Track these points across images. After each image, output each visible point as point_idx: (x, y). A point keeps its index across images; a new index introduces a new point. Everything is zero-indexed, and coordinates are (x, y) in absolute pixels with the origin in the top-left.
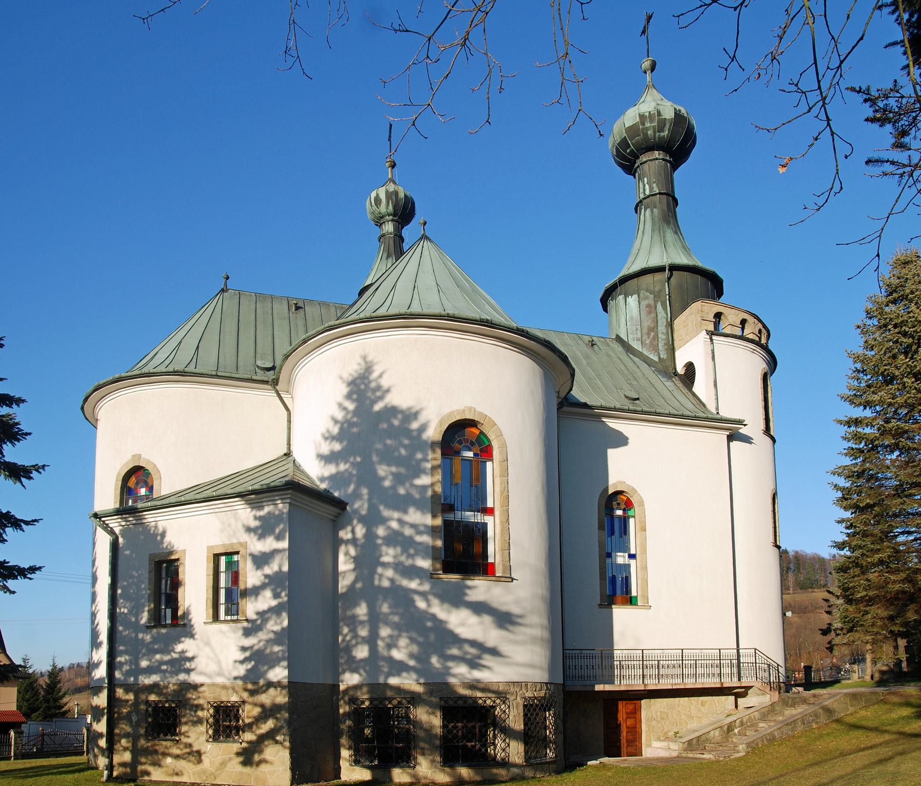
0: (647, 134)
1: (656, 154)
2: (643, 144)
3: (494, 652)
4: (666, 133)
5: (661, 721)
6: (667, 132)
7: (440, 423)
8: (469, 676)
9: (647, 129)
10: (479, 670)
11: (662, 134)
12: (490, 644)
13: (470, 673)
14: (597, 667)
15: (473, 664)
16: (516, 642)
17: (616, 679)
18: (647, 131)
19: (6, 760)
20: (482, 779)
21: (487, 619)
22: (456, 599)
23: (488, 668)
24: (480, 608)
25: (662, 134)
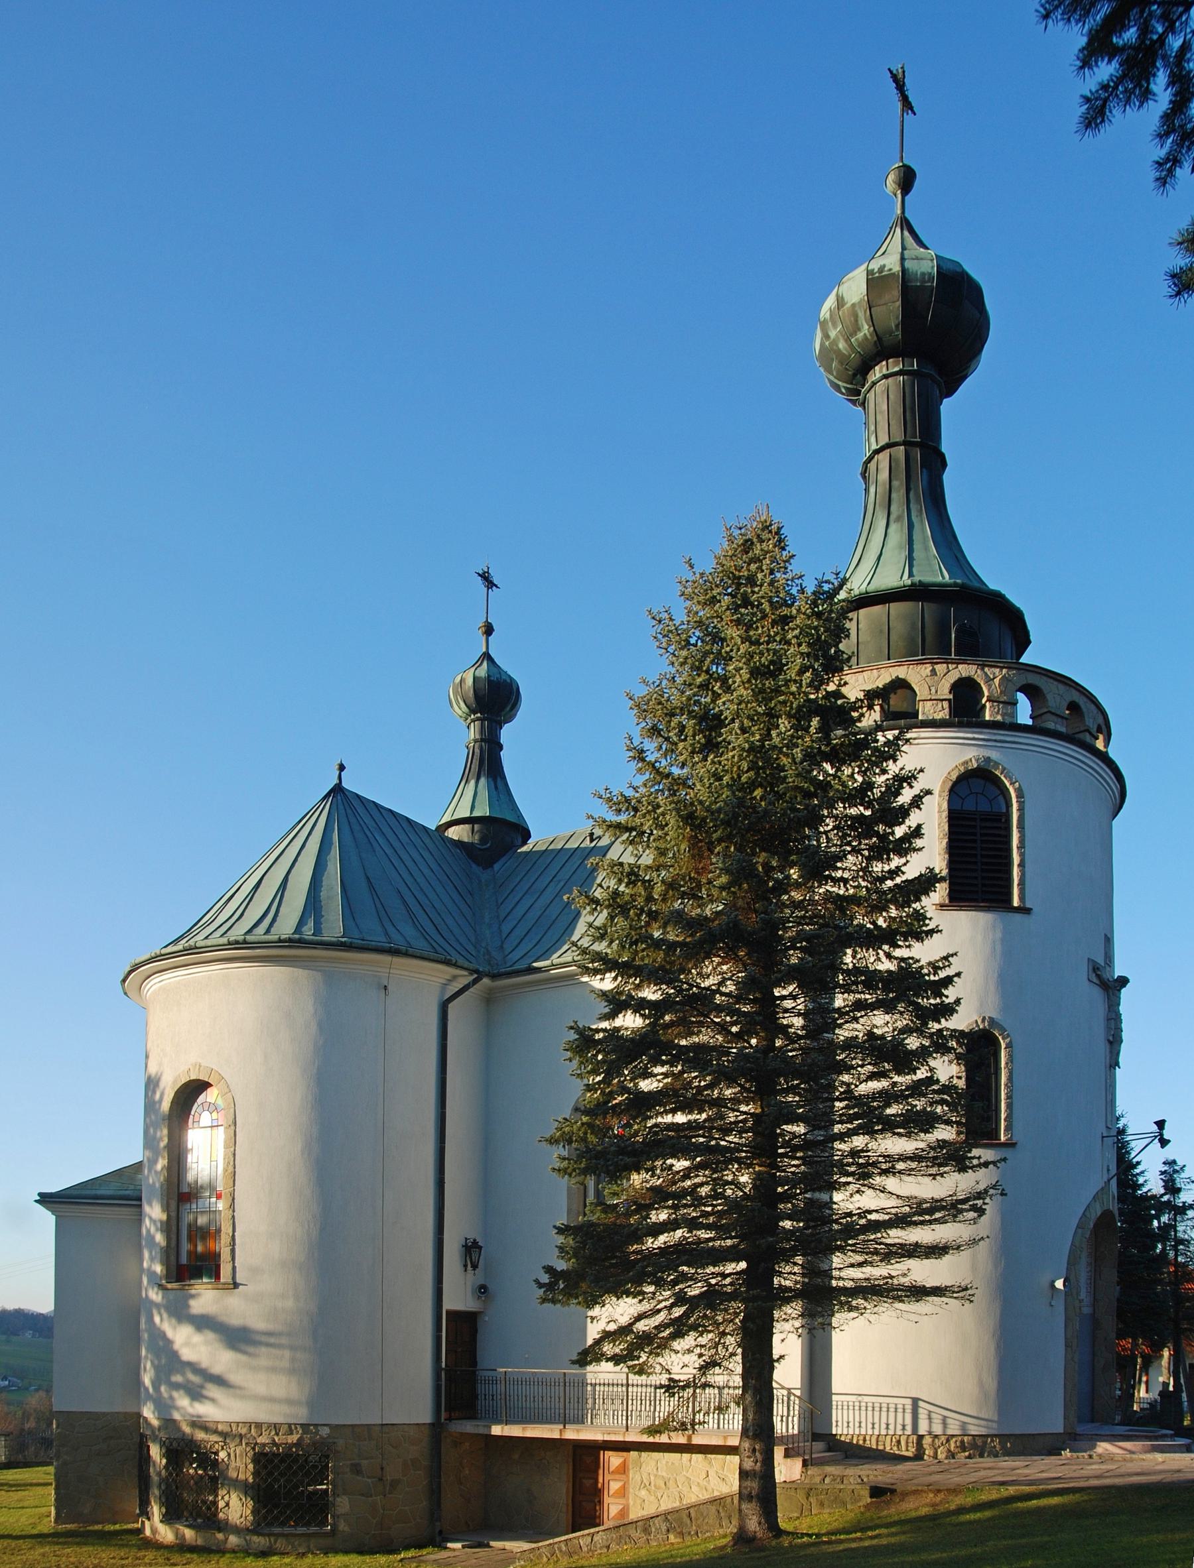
0: (839, 350)
1: (878, 371)
2: (847, 369)
3: (220, 1381)
4: (866, 329)
5: (655, 1492)
6: (866, 327)
7: (175, 1082)
8: (190, 1410)
9: (835, 342)
10: (201, 1402)
11: (860, 335)
12: (216, 1370)
13: (191, 1405)
14: (499, 1397)
15: (196, 1395)
16: (254, 1369)
17: (797, 1412)
18: (837, 346)
19: (653, 1451)
20: (203, 1544)
21: (210, 1335)
22: (180, 1313)
23: (213, 1400)
24: (203, 1323)
25: (860, 335)
